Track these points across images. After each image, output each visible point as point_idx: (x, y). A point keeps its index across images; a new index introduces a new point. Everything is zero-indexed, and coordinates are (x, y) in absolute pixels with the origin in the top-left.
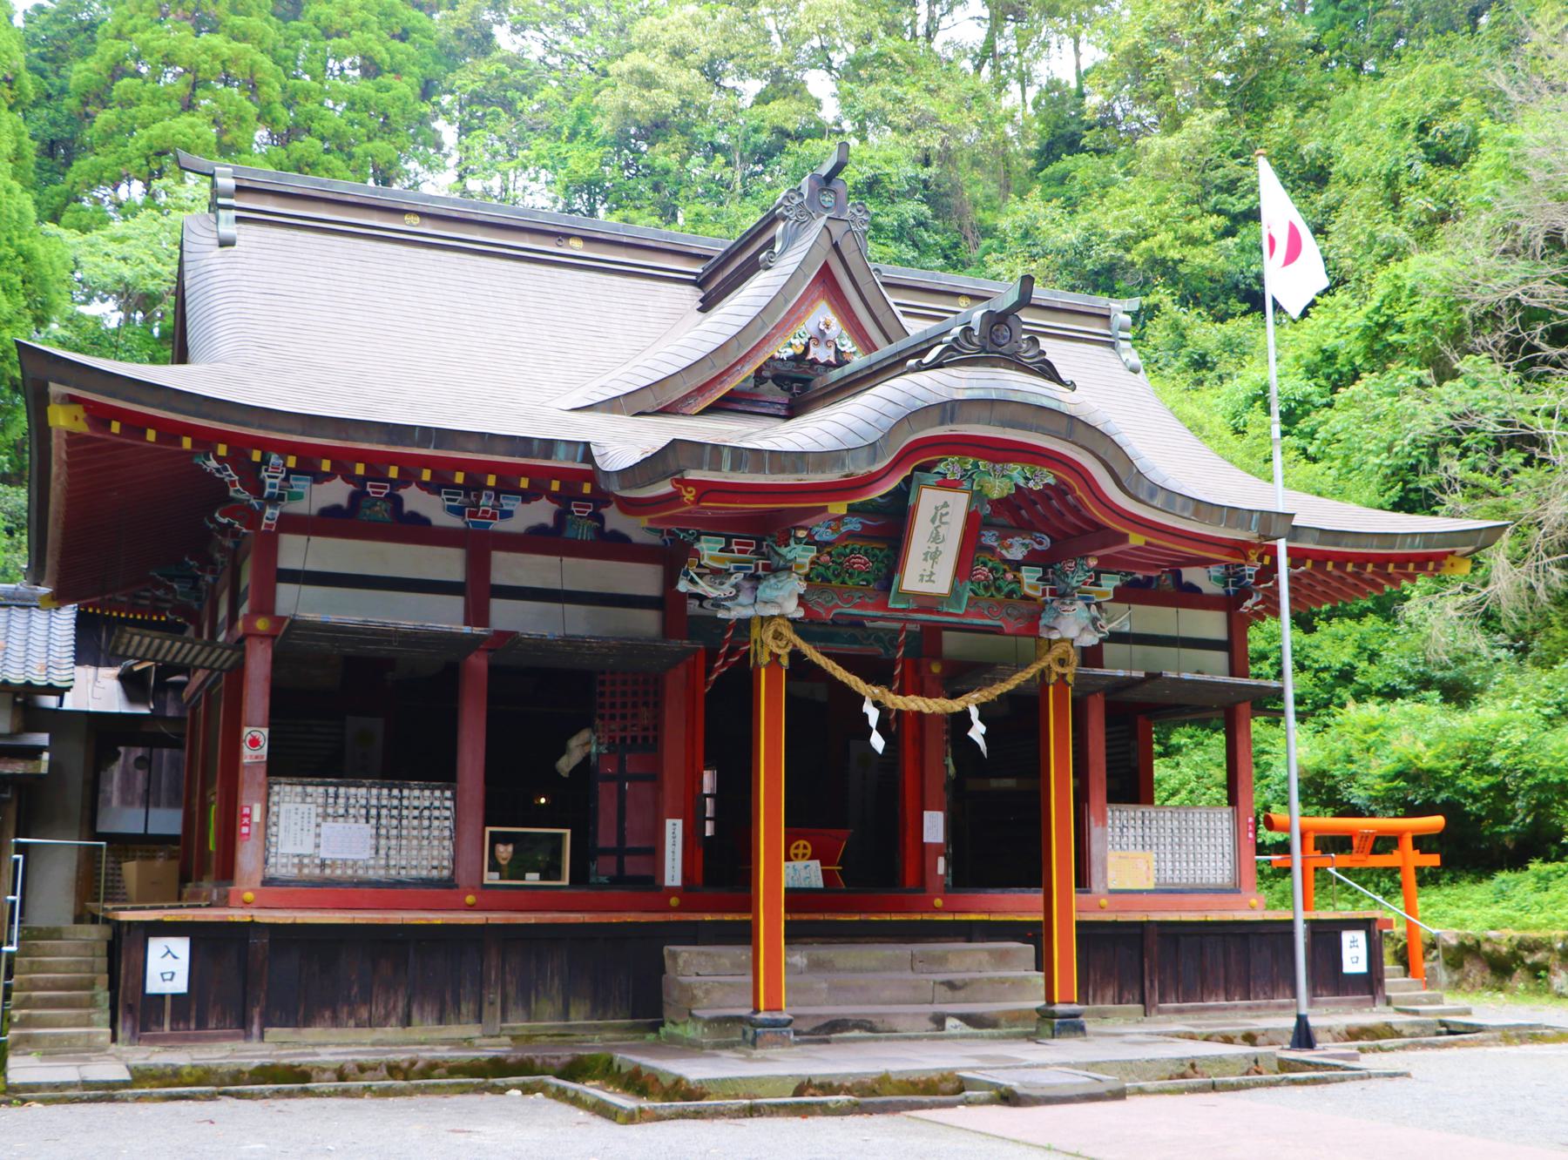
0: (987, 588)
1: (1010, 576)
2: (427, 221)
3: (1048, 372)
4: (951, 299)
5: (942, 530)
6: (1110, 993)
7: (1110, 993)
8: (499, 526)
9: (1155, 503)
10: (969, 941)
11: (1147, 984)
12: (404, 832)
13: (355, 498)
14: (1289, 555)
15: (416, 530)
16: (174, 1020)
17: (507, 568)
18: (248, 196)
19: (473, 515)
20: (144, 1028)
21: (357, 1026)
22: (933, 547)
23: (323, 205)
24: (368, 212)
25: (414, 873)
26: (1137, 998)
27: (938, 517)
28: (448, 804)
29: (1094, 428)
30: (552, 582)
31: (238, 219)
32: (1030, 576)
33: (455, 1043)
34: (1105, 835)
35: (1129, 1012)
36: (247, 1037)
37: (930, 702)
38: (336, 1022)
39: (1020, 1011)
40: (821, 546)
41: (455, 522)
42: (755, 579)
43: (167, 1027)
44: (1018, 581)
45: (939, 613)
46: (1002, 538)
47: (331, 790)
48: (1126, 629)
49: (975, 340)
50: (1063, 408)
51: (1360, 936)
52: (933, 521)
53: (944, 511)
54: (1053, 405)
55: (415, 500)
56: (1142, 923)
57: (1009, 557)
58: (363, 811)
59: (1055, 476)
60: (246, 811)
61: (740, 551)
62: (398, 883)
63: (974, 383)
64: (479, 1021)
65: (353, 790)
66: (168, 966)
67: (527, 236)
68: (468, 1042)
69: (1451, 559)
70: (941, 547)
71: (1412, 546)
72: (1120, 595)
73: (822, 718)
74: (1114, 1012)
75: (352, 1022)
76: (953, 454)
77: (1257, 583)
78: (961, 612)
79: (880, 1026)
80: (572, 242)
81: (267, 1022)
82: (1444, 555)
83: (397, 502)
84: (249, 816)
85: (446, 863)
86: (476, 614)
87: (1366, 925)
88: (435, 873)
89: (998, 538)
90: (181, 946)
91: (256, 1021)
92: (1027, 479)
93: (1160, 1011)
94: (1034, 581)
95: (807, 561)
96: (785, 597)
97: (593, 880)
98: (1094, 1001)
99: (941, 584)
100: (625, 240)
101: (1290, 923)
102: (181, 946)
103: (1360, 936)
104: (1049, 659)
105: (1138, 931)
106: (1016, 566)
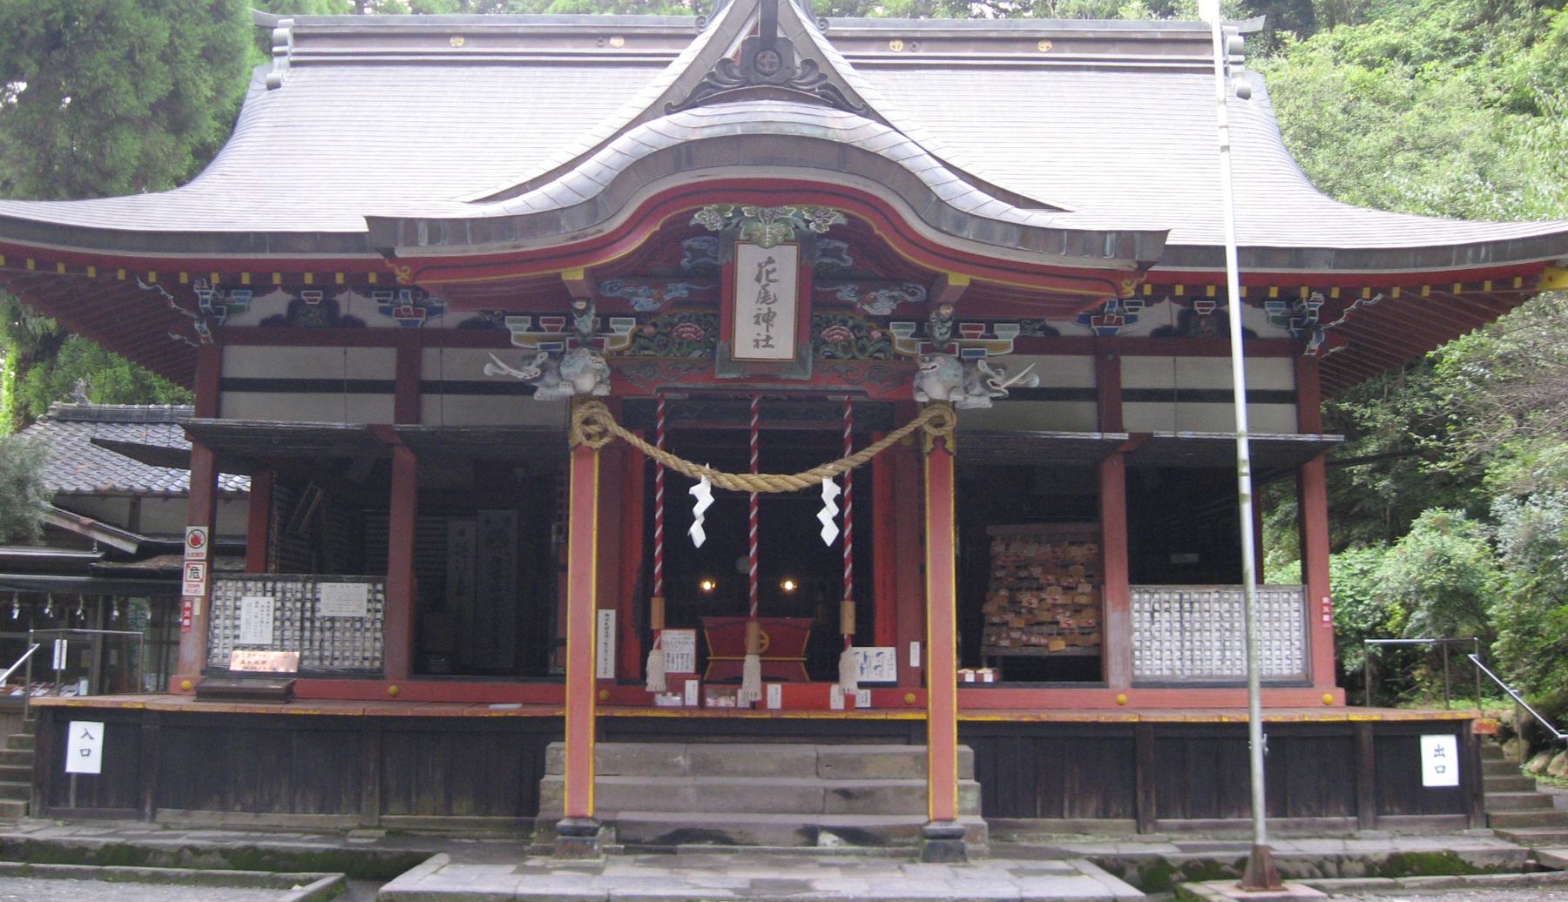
0: (846, 349)
1: (876, 334)
2: (471, 41)
3: (839, 97)
4: (1031, 46)
5: (772, 289)
6: (1092, 806)
7: (1092, 806)
8: (435, 323)
9: (965, 234)
10: (909, 743)
11: (1141, 796)
12: (1197, 625)
13: (1185, 317)
14: (1241, 283)
15: (351, 333)
16: (79, 797)
17: (1137, 372)
18: (307, 42)
19: (1099, 322)
20: (53, 802)
21: (244, 810)
22: (764, 309)
23: (328, 41)
24: (1012, 46)
25: (347, 664)
26: (1129, 810)
27: (764, 273)
28: (380, 596)
29: (875, 155)
30: (1166, 383)
31: (294, 64)
32: (900, 334)
33: (326, 834)
34: (1127, 620)
35: (1118, 828)
36: (140, 817)
37: (792, 478)
38: (224, 806)
39: (910, 826)
40: (642, 318)
41: (390, 322)
42: (557, 357)
43: (72, 804)
44: (888, 339)
45: (778, 380)
46: (861, 293)
47: (269, 585)
48: (1036, 382)
49: (736, 72)
50: (831, 136)
51: (1449, 743)
52: (758, 279)
53: (769, 267)
54: (818, 133)
55: (353, 305)
56: (1133, 724)
57: (872, 312)
58: (298, 605)
59: (846, 216)
60: (188, 604)
61: (550, 329)
62: (331, 674)
63: (716, 120)
64: (358, 810)
65: (289, 585)
66: (85, 749)
67: (568, 42)
68: (341, 834)
69: (1549, 272)
70: (774, 307)
71: (1476, 259)
72: (1022, 346)
73: (644, 502)
74: (1096, 827)
75: (238, 808)
76: (709, 203)
77: (1321, 321)
78: (808, 377)
79: (735, 837)
80: (614, 41)
81: (159, 803)
82: (1540, 268)
83: (332, 307)
84: (190, 609)
85: (377, 655)
86: (408, 410)
87: (1454, 727)
88: (367, 664)
89: (858, 293)
90: (97, 729)
91: (149, 800)
92: (807, 222)
93: (1159, 828)
94: (908, 338)
95: (627, 334)
96: (585, 375)
97: (551, 671)
98: (1071, 814)
99: (783, 348)
100: (665, 31)
101: (1244, 727)
102: (97, 729)
103: (1449, 743)
104: (922, 421)
105: (1349, 732)
106: (884, 322)
